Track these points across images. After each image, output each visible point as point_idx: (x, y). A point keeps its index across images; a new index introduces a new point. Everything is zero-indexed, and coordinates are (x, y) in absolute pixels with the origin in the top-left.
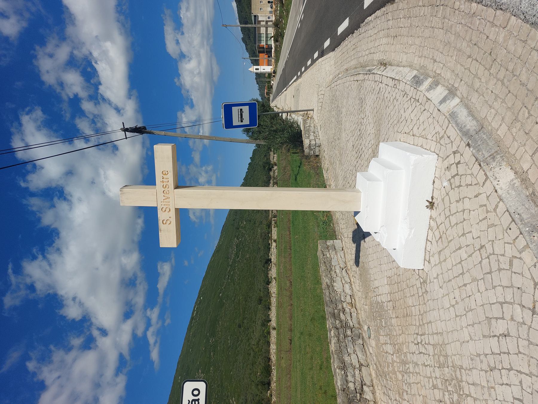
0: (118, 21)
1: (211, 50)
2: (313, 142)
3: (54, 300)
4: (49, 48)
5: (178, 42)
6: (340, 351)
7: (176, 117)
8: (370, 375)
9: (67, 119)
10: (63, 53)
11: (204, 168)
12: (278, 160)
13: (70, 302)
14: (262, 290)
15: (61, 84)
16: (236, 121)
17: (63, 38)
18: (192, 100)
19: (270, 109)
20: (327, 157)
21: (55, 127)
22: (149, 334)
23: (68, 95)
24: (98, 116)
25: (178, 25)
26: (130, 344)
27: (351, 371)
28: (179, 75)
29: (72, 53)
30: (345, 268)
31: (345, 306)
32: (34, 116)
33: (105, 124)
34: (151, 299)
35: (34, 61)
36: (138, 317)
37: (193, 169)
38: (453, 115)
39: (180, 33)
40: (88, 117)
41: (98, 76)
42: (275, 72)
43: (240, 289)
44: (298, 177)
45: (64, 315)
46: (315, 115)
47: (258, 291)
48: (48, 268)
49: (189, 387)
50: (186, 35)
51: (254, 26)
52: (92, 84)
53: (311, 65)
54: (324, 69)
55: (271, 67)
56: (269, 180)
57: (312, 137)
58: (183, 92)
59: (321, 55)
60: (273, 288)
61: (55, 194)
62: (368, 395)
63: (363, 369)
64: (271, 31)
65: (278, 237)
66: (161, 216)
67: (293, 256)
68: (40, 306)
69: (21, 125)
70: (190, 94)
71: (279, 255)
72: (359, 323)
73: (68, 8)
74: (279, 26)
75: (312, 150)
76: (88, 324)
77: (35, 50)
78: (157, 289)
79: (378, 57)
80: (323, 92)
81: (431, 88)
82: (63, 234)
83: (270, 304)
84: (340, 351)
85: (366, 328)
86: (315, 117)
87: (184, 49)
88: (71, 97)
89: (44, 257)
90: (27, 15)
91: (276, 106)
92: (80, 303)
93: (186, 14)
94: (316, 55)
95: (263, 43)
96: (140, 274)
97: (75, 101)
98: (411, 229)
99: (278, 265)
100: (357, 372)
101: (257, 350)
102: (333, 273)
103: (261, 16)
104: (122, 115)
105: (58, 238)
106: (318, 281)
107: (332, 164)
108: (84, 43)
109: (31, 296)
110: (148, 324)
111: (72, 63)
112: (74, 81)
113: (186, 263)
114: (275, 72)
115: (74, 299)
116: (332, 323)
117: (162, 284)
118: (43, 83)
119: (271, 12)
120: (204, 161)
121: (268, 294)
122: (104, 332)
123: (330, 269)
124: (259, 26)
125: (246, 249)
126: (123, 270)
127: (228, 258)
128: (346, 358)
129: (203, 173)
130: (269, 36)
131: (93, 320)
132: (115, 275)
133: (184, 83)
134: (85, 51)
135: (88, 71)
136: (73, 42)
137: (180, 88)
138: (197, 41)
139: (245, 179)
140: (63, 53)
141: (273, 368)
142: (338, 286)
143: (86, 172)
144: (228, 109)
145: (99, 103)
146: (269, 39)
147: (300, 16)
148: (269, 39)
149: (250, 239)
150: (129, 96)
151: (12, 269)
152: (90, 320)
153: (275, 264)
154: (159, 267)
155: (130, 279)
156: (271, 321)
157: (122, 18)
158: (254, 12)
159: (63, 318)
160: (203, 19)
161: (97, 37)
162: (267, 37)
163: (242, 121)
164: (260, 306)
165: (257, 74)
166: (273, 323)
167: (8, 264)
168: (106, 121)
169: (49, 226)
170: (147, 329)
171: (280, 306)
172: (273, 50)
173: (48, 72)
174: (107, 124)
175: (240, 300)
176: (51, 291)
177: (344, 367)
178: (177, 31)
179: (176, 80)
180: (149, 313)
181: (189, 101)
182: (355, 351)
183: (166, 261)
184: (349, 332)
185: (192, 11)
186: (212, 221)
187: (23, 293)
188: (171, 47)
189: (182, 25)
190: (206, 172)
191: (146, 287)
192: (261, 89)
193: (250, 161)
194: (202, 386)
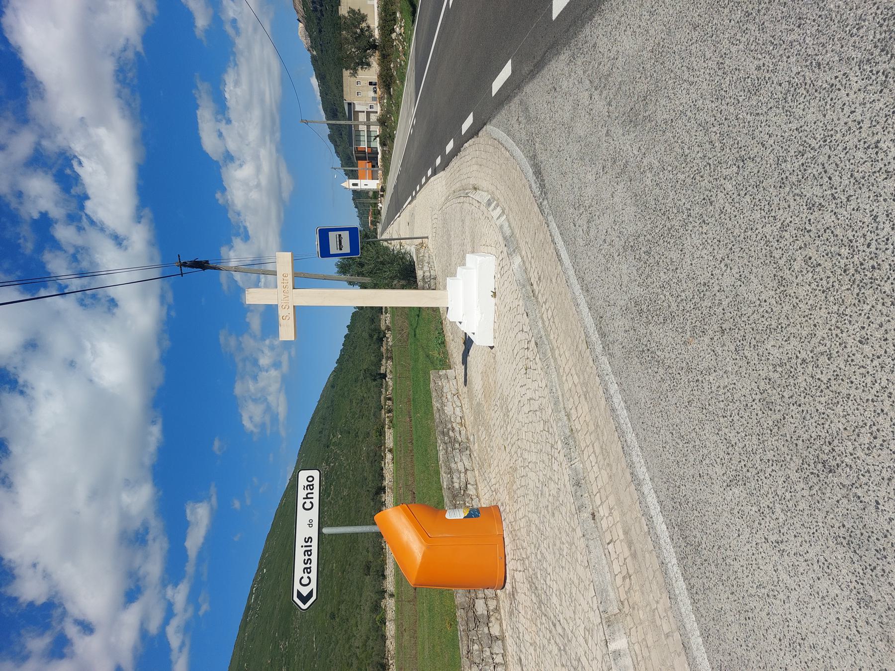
1: (278, 150)
2: (427, 274)
6: (448, 460)
10: (23, 144)
11: (267, 342)
12: (392, 322)
15: (20, 195)
16: (333, 249)
17: (23, 119)
18: (245, 228)
19: (376, 243)
22: (171, 630)
24: (83, 248)
25: (221, 108)
26: (135, 649)
28: (224, 190)
29: (38, 144)
31: (454, 425)
36: (150, 598)
37: (249, 342)
38: (501, 227)
39: (224, 122)
40: (65, 252)
42: (383, 189)
43: (333, 550)
45: (14, 595)
46: (430, 243)
47: (365, 553)
49: (303, 475)
50: (235, 123)
51: (349, 122)
52: (74, 196)
53: (425, 183)
54: (436, 188)
55: (378, 181)
56: (381, 360)
58: (230, 215)
59: (434, 173)
63: (468, 472)
64: (376, 130)
66: (281, 312)
70: (242, 218)
72: (468, 439)
73: (32, 73)
74: (387, 122)
75: (426, 283)
76: (60, 610)
78: (185, 550)
79: (472, 181)
80: (436, 216)
82: (16, 448)
84: (448, 460)
86: (430, 246)
87: (232, 146)
88: (35, 217)
93: (235, 90)
94: (430, 172)
95: (364, 145)
96: (156, 525)
97: (44, 223)
98: (482, 314)
100: (462, 475)
101: (363, 656)
102: (444, 399)
103: (359, 104)
104: (126, 249)
106: (429, 403)
110: (169, 613)
112: (41, 193)
113: (237, 504)
114: (383, 189)
115: (34, 565)
117: (194, 541)
119: (374, 99)
122: (87, 628)
123: (441, 396)
124: (356, 123)
125: (342, 481)
126: (125, 516)
128: (453, 465)
129: (266, 351)
130: (373, 134)
131: (69, 607)
132: (110, 524)
133: (233, 201)
135: (64, 171)
136: (40, 126)
137: (224, 209)
138: (253, 134)
139: (338, 361)
140: (23, 144)
141: (391, 662)
142: (448, 410)
143: (60, 343)
144: (324, 234)
147: (412, 121)
150: (138, 218)
152: (61, 605)
154: (188, 512)
155: (137, 533)
157: (126, 91)
158: (348, 97)
160: (262, 101)
162: (369, 136)
163: (341, 249)
165: (354, 191)
170: (166, 621)
172: (379, 156)
175: (332, 570)
177: (450, 472)
178: (219, 117)
179: (218, 195)
181: (242, 230)
184: (457, 446)
185: (245, 86)
186: (283, 433)
188: (209, 142)
190: (272, 348)
192: (362, 215)
193: (346, 331)
194: (316, 474)
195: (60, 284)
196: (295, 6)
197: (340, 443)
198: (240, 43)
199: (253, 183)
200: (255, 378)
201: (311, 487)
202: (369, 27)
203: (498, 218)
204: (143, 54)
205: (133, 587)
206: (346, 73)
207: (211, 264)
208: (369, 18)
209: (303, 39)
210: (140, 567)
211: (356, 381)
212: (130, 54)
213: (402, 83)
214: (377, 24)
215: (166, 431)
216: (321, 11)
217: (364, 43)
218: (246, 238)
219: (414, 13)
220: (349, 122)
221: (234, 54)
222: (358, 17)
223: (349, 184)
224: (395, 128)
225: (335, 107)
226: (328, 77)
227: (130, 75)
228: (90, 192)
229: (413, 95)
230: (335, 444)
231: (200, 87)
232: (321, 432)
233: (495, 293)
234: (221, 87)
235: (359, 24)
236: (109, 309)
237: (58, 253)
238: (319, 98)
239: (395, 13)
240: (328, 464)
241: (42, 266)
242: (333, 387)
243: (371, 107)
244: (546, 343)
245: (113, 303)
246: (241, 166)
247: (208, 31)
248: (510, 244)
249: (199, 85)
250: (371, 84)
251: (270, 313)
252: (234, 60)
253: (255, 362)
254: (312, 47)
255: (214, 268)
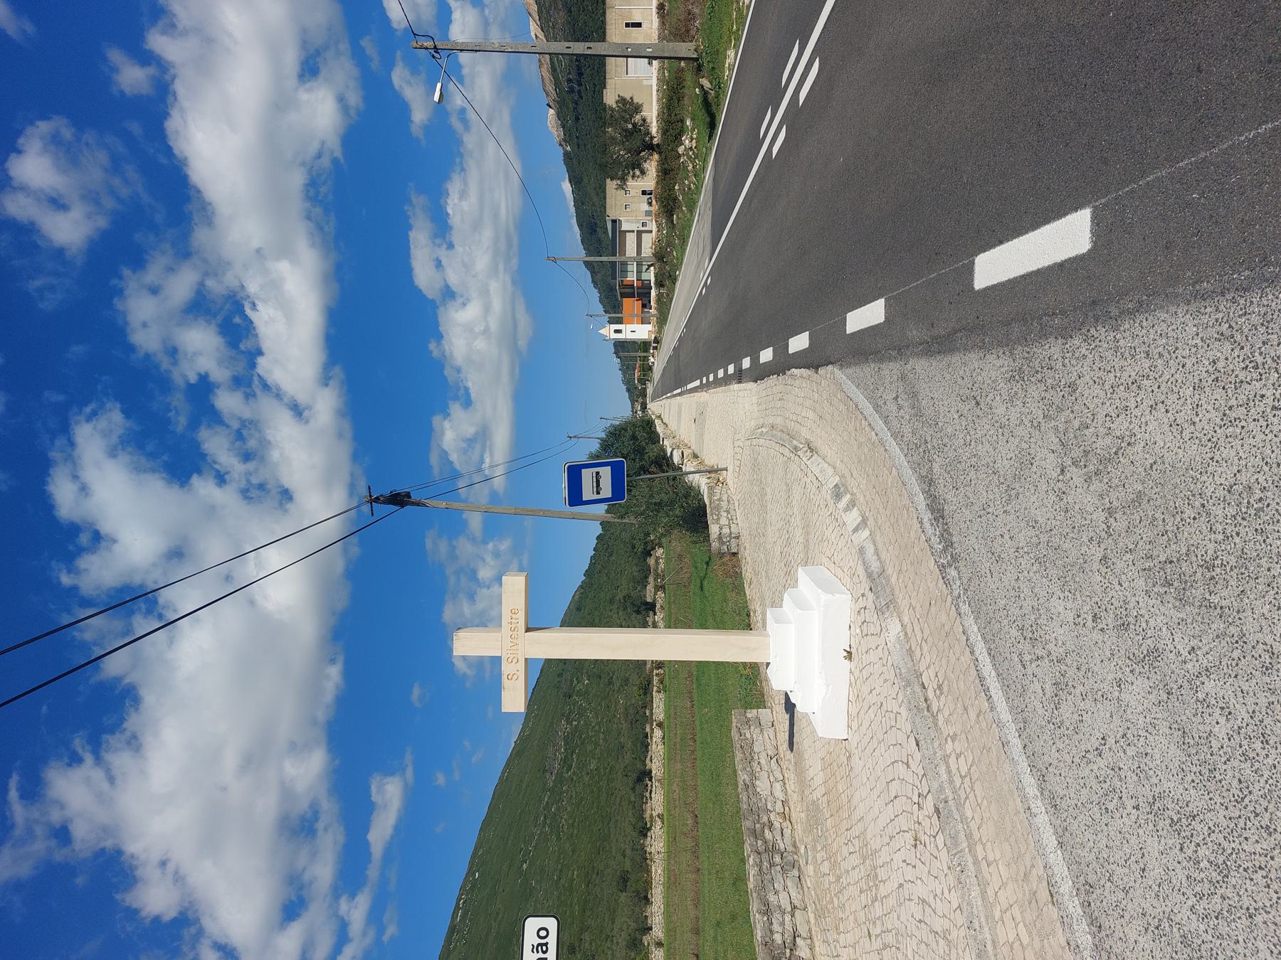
0: (308, 218)
1: (514, 283)
2: (726, 531)
3: (113, 869)
4: (153, 274)
5: (439, 264)
6: (762, 888)
7: (430, 430)
8: (808, 922)
9: (180, 429)
11: (490, 546)
13: (149, 872)
14: (628, 852)
15: (173, 352)
16: (588, 493)
17: (184, 252)
18: (467, 389)
20: (749, 559)
21: (150, 448)
23: (184, 376)
24: (251, 422)
25: (442, 228)
27: (779, 916)
28: (439, 337)
29: (201, 284)
30: (776, 757)
31: (772, 818)
32: (102, 423)
33: (265, 444)
34: (350, 876)
35: (115, 301)
36: (316, 914)
37: (465, 547)
38: (862, 551)
39: (445, 246)
41: (256, 336)
43: (573, 851)
44: (705, 583)
45: (134, 906)
46: (729, 477)
48: (105, 785)
49: (532, 925)
51: (612, 259)
52: (243, 352)
55: (649, 327)
56: (646, 577)
57: (724, 521)
58: (447, 372)
59: (740, 376)
60: (657, 843)
61: (135, 601)
62: (803, 951)
63: (797, 913)
65: (668, 716)
66: (506, 668)
67: (699, 754)
68: (80, 881)
69: (72, 444)
70: (462, 376)
71: (670, 759)
72: (795, 846)
73: (199, 191)
74: (667, 261)
75: (724, 543)
76: (193, 930)
77: (121, 278)
81: (847, 509)
82: (149, 697)
83: (648, 884)
84: (762, 888)
85: (802, 850)
87: (453, 279)
88: (192, 381)
89: (98, 760)
90: (109, 203)
91: (659, 417)
92: (176, 872)
93: (461, 204)
95: (632, 277)
96: (328, 807)
97: (202, 389)
99: (668, 782)
100: (788, 918)
102: (755, 764)
103: (628, 221)
104: (307, 422)
105: (137, 709)
107: (757, 574)
108: (229, 263)
109: (60, 856)
111: (199, 306)
112: (201, 347)
113: (441, 779)
115: (163, 864)
116: (751, 845)
117: (380, 832)
118: (131, 348)
119: (648, 213)
120: (491, 531)
121: (643, 861)
124: (623, 259)
125: (589, 748)
126: (287, 794)
127: (545, 771)
128: (772, 898)
129: (489, 559)
131: (207, 923)
132: (267, 807)
134: (230, 280)
135: (233, 321)
136: (205, 261)
137: (438, 365)
138: (482, 261)
139: (587, 573)
140: (182, 286)
142: (762, 786)
145: (254, 395)
146: (645, 268)
147: (704, 277)
148: (645, 268)
149: (598, 723)
150: (325, 380)
151: (18, 790)
152: (197, 920)
153: (659, 781)
155: (303, 818)
156: (651, 929)
157: (318, 211)
158: (613, 212)
159: (133, 913)
160: (496, 216)
161: (258, 251)
163: (598, 493)
164: (623, 897)
166: (658, 932)
167: (11, 777)
168: (270, 434)
169: (118, 679)
171: (672, 882)
173: (145, 325)
174: (269, 442)
175: (573, 880)
176: (108, 844)
177: (767, 911)
178: (438, 241)
179: (432, 346)
180: (344, 906)
182: (785, 887)
183: (390, 772)
184: (777, 859)
185: (473, 198)
187: (40, 846)
188: (424, 276)
189: (451, 228)
190: (497, 555)
191: (341, 838)
194: (551, 924)
195: (218, 471)
196: (544, 86)
197: (587, 692)
198: (470, 140)
199: (479, 328)
200: (472, 597)
201: (543, 947)
202: (644, 120)
203: (856, 530)
204: (342, 161)
205: (294, 899)
206: (611, 185)
207: (415, 497)
208: (645, 107)
209: (554, 131)
210: (304, 869)
211: (611, 601)
212: (326, 162)
213: (691, 210)
214: (655, 113)
215: (348, 673)
216: (579, 92)
217: (636, 143)
218: (468, 403)
219: (712, 126)
220: (612, 259)
221: (461, 155)
222: (630, 107)
223: (609, 331)
224: (678, 266)
225: (598, 234)
226: (585, 180)
227: (323, 189)
228: (265, 346)
229: (708, 249)
230: (579, 693)
231: (414, 200)
232: (560, 675)
233: (850, 653)
234: (442, 201)
235: (631, 117)
236: (281, 504)
237: (219, 429)
238: (573, 210)
239: (682, 121)
240: (569, 722)
241: (196, 446)
242: (579, 609)
243: (644, 224)
244: (957, 816)
245: (286, 495)
246: (464, 304)
247: (427, 128)
248: (878, 591)
249: (413, 198)
250: (644, 193)
251: (490, 669)
252: (461, 164)
253: (473, 575)
254: (565, 140)
255: (418, 504)
